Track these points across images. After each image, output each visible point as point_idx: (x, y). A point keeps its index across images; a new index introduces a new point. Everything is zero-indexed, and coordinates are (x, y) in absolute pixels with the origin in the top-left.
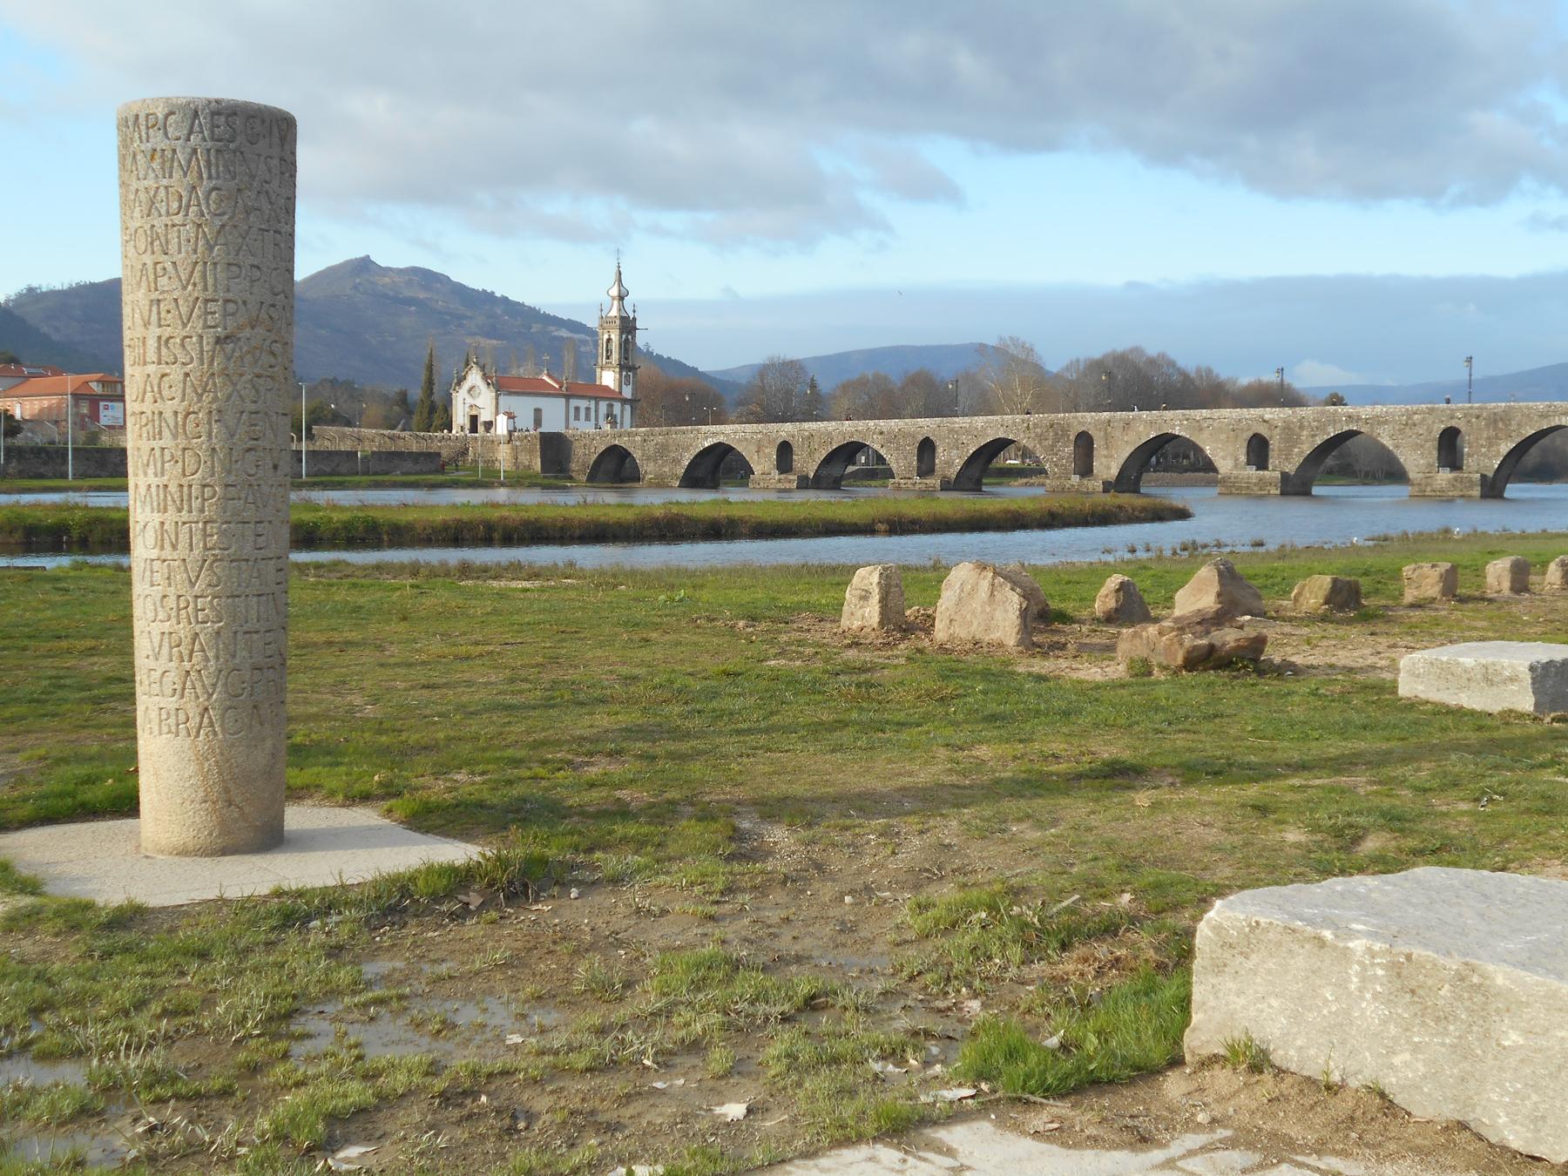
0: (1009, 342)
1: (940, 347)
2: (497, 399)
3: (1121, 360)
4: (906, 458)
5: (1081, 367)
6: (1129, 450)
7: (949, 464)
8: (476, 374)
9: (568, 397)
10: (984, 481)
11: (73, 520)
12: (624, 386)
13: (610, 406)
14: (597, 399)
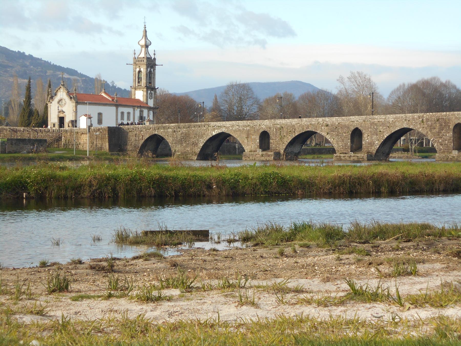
0: (357, 75)
1: (274, 84)
2: (76, 107)
3: (426, 84)
4: (343, 141)
8: (63, 91)
9: (117, 106)
11: (28, 177)
12: (149, 100)
13: (141, 112)
14: (133, 107)
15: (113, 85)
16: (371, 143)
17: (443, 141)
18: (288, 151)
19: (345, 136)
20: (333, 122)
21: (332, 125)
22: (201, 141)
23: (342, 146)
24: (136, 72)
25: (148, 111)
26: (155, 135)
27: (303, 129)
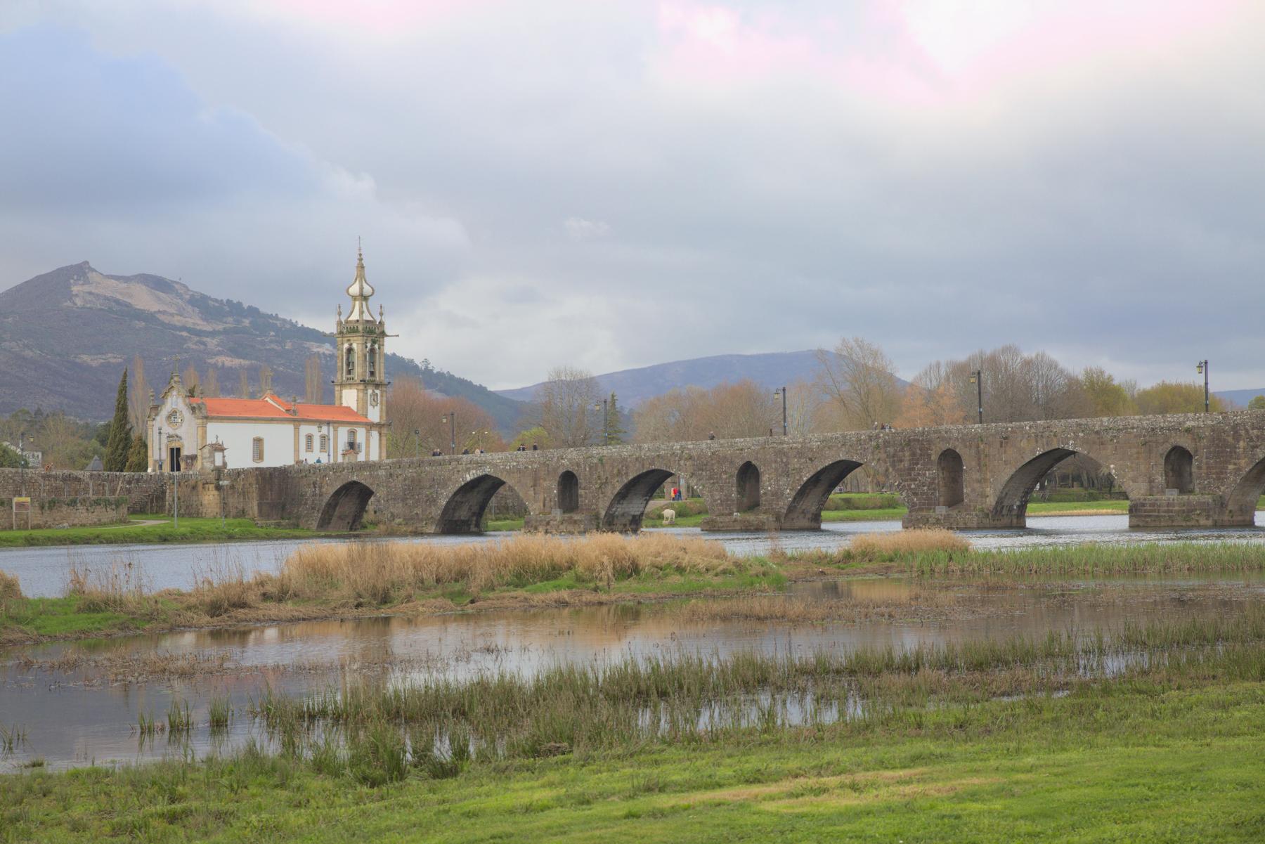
4: (722, 489)
12: (370, 408)
15: (427, 368)
18: (616, 511)
21: (699, 457)
22: (442, 493)
23: (720, 499)
25: (368, 431)
27: (643, 467)
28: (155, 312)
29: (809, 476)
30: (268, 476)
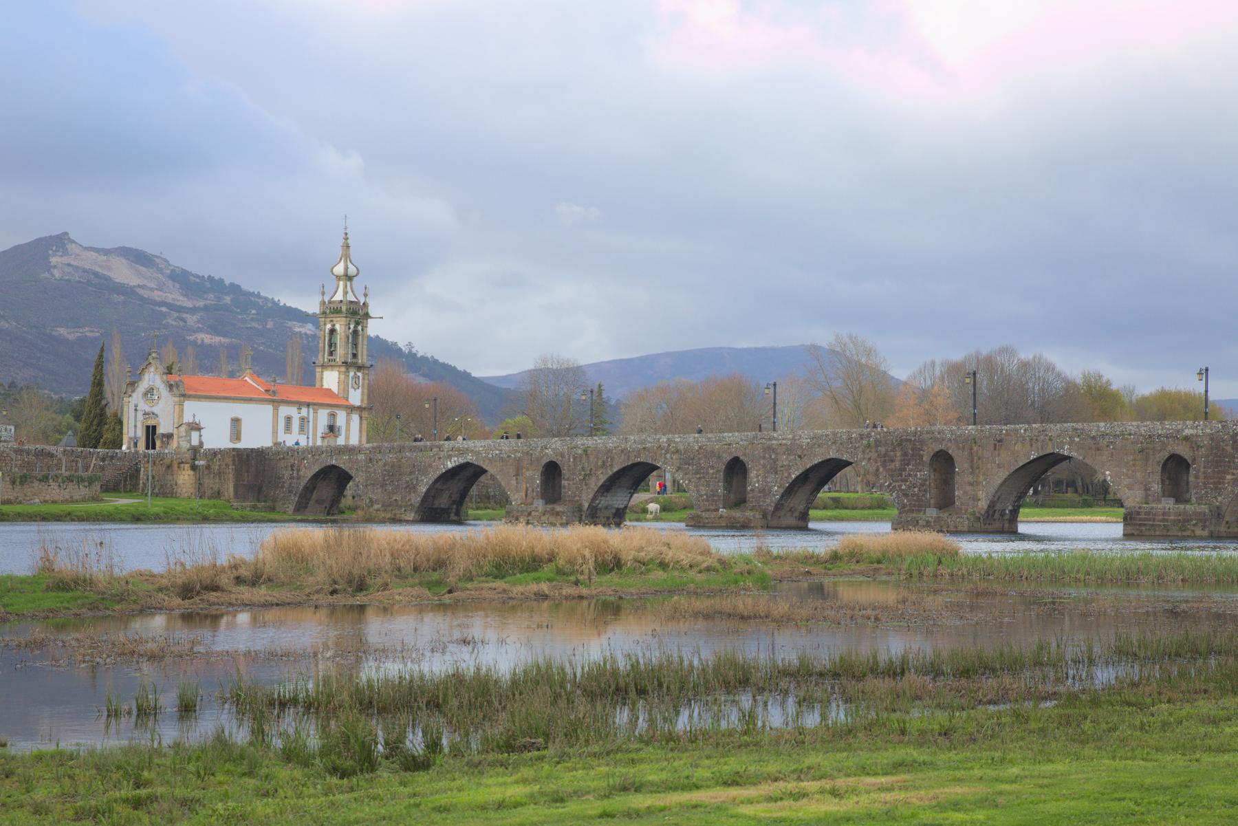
2: (1206, 391)
4: (708, 484)
5: (938, 372)
6: (1002, 475)
7: (765, 492)
10: (811, 512)
12: (351, 391)
15: (410, 351)
16: (764, 489)
17: (909, 487)
18: (599, 504)
19: (713, 473)
20: (689, 444)
21: (686, 451)
22: (422, 480)
23: (705, 494)
24: (325, 331)
25: (348, 414)
26: (333, 466)
28: (134, 286)
29: (798, 473)
30: (245, 457)
